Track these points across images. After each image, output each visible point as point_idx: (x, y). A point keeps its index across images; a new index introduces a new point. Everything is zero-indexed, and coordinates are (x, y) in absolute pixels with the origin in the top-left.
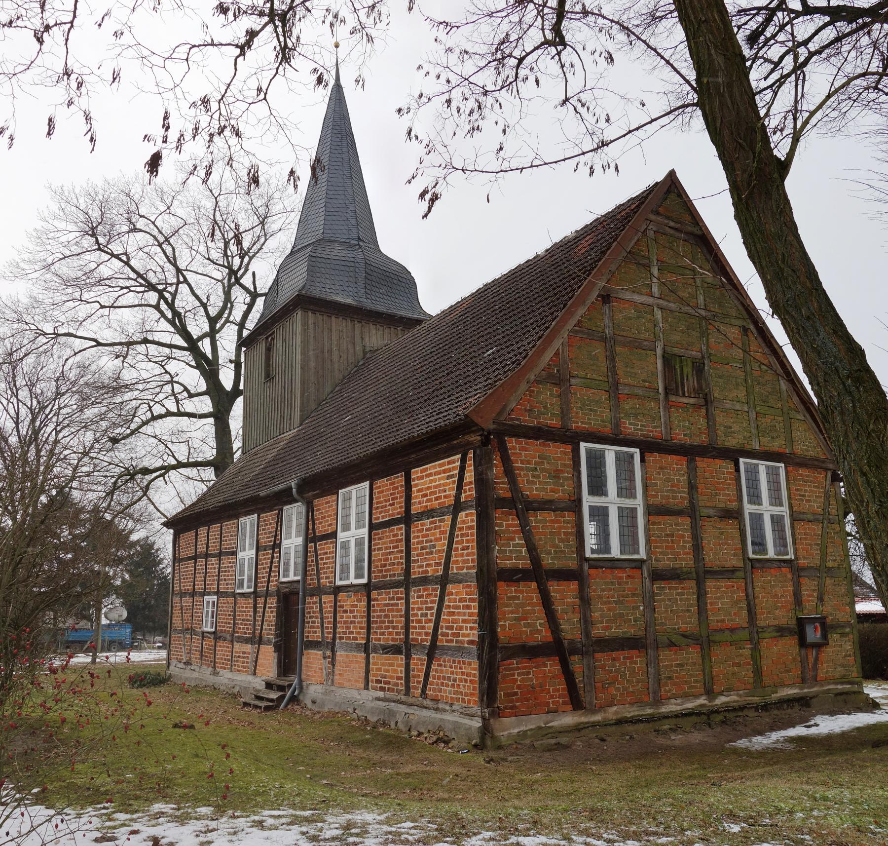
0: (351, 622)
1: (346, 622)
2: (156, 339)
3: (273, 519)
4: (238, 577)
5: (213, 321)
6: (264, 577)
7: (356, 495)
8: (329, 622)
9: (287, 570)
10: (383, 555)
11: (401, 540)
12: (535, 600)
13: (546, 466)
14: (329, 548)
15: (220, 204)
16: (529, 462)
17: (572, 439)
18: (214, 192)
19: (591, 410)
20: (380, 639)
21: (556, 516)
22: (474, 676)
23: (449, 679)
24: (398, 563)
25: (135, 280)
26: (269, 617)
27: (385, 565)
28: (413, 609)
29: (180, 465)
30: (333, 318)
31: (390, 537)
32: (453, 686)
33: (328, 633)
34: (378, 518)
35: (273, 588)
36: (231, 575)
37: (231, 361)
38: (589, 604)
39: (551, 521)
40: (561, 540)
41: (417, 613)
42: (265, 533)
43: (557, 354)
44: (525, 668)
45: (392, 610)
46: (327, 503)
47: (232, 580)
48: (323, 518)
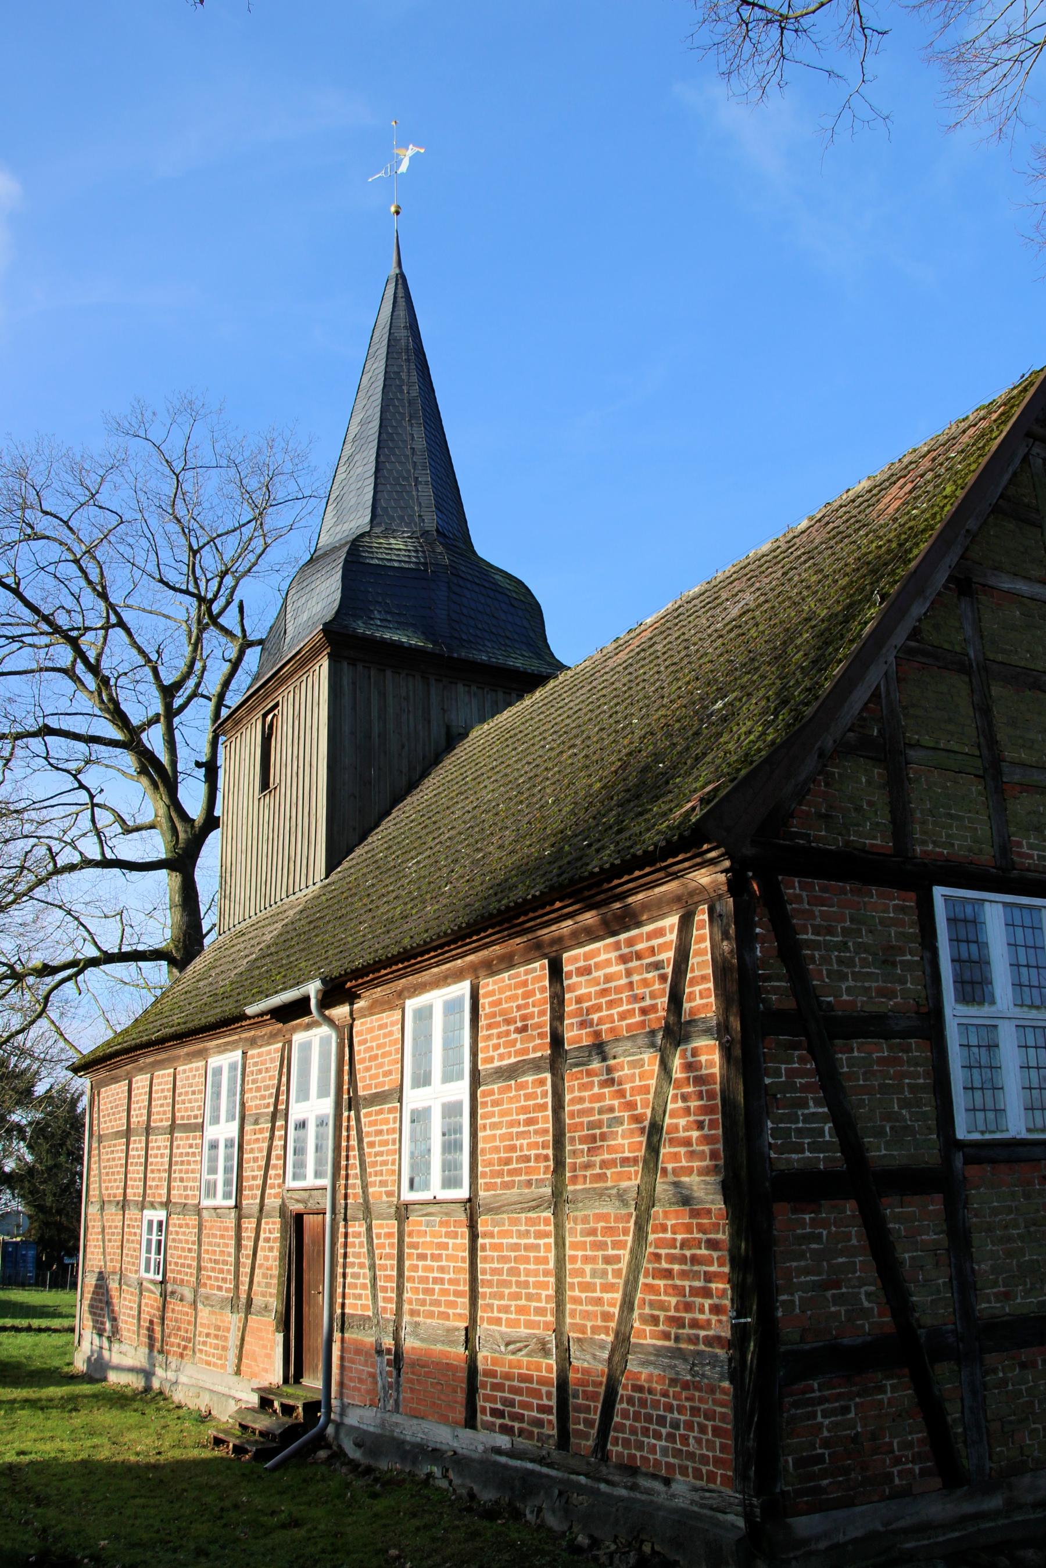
0: (436, 1281)
1: (424, 1280)
2: (64, 727)
3: (272, 1060)
4: (206, 1176)
5: (168, 692)
6: (254, 1178)
7: (438, 1002)
8: (388, 1278)
9: (300, 1165)
10: (502, 1138)
11: (543, 1107)
12: (854, 1242)
13: (866, 939)
14: (386, 1121)
15: (186, 487)
16: (830, 931)
17: (915, 877)
18: (174, 464)
19: (950, 816)
20: (498, 1321)
21: (890, 1048)
22: (723, 1416)
23: (661, 1421)
24: (537, 1156)
25: (35, 625)
26: (266, 1258)
27: (508, 1161)
28: (574, 1259)
29: (109, 958)
30: (389, 673)
31: (517, 1099)
32: (671, 1437)
33: (385, 1300)
34: (491, 1060)
35: (272, 1202)
36: (193, 1171)
37: (198, 765)
38: (969, 1244)
39: (881, 1061)
40: (905, 1104)
41: (582, 1268)
42: (258, 1089)
43: (876, 695)
44: (839, 1397)
45: (526, 1259)
46: (381, 1027)
47: (194, 1180)
48: (374, 1058)
